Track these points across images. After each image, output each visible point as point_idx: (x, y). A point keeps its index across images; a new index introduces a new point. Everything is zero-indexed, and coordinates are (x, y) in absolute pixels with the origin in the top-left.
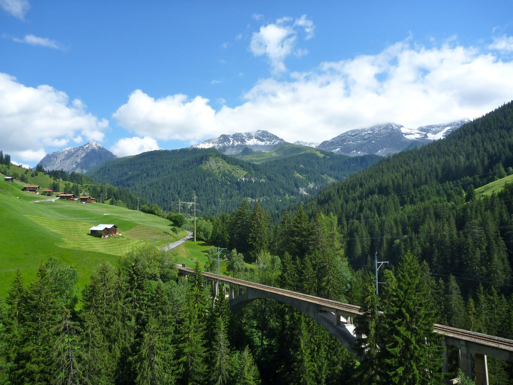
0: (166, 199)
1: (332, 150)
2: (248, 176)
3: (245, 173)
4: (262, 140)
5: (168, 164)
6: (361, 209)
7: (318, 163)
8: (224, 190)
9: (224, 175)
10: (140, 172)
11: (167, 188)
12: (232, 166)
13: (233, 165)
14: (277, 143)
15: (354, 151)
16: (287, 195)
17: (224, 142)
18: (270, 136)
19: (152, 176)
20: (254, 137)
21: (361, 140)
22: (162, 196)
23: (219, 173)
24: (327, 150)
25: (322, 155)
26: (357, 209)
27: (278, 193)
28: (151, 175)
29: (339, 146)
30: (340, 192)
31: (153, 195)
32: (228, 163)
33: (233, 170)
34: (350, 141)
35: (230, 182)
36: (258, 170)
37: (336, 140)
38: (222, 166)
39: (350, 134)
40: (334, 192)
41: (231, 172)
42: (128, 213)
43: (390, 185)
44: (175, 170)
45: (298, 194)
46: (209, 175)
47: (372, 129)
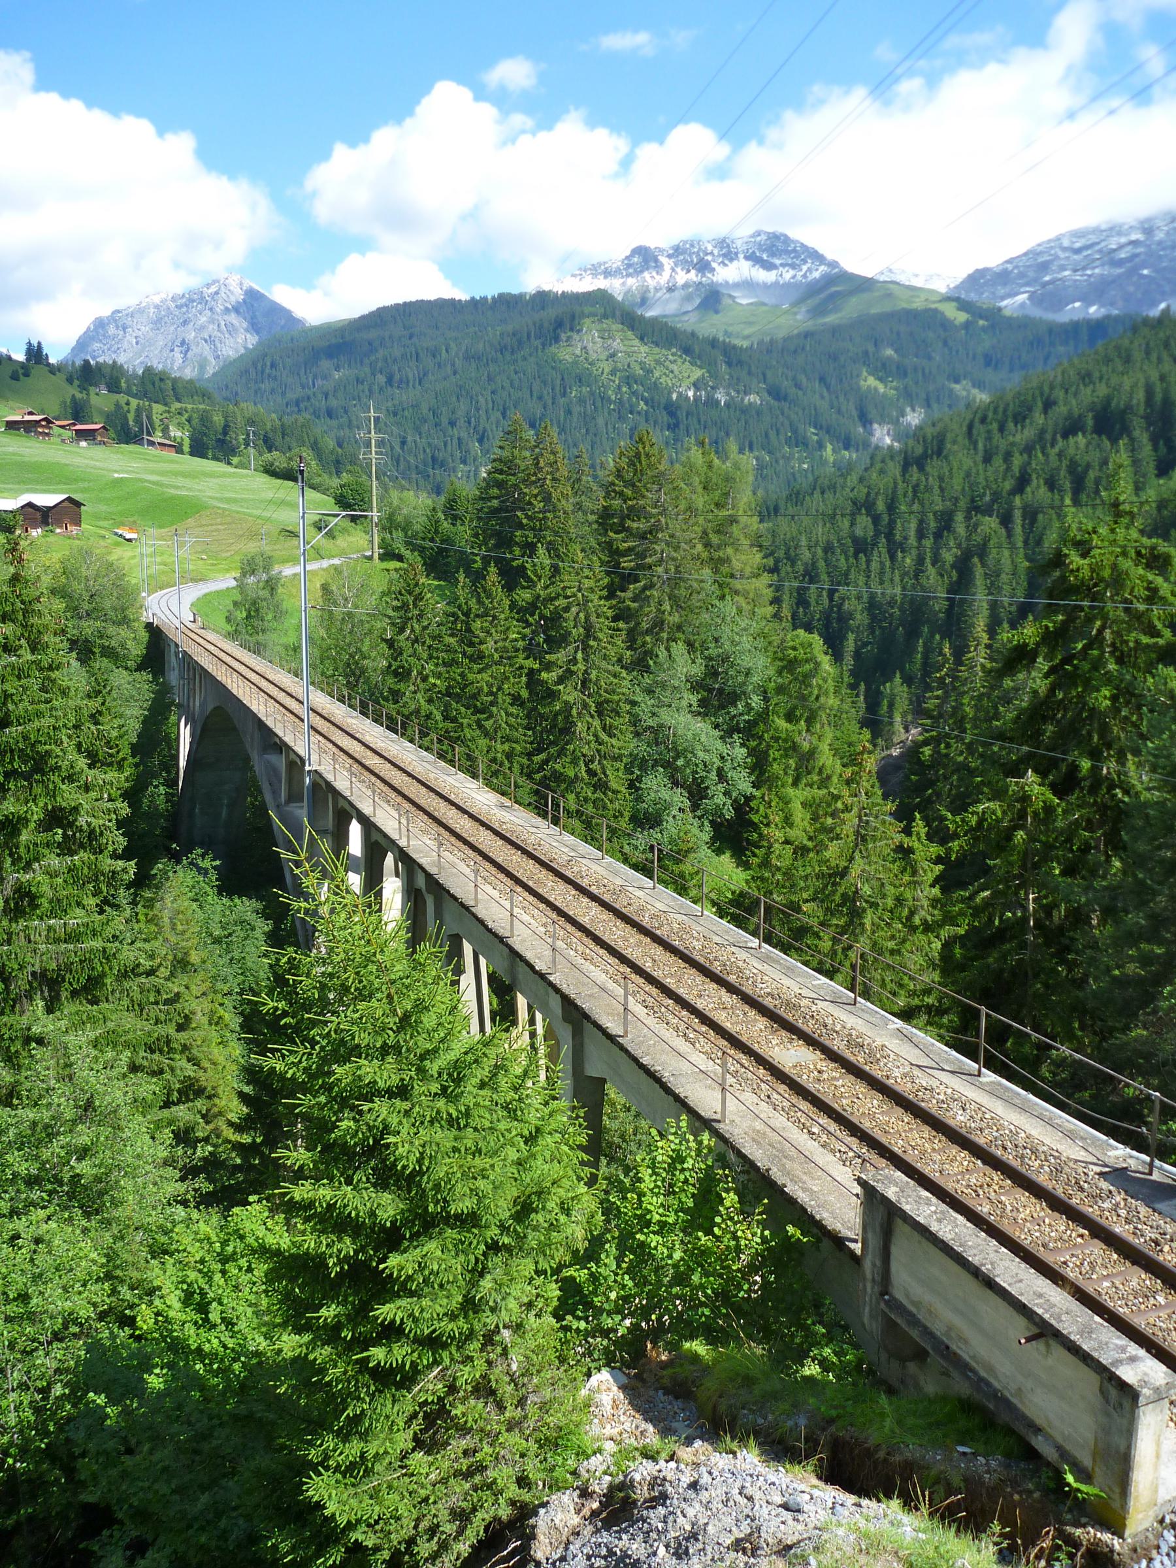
0: (440, 455)
1: (1003, 298)
2: (706, 385)
3: (697, 373)
4: (769, 266)
5: (453, 345)
6: (1022, 482)
7: (945, 343)
8: (625, 428)
9: (629, 380)
10: (367, 370)
11: (445, 421)
12: (657, 350)
13: (657, 345)
14: (816, 275)
15: (1077, 304)
16: (829, 447)
17: (642, 272)
18: (794, 250)
19: (404, 383)
20: (741, 256)
21: (1103, 265)
22: (430, 445)
23: (613, 372)
24: (983, 299)
25: (962, 317)
26: (1008, 485)
27: (799, 441)
28: (401, 381)
29: (1027, 284)
30: (975, 432)
31: (403, 443)
32: (642, 339)
33: (658, 362)
34: (1063, 268)
35: (646, 404)
36: (740, 363)
37: (1016, 267)
38: (623, 348)
39: (1066, 243)
40: (957, 429)
41: (649, 371)
42: (224, 475)
43: (1134, 402)
44: (474, 365)
45: (866, 444)
46: (580, 380)
47: (1147, 227)
